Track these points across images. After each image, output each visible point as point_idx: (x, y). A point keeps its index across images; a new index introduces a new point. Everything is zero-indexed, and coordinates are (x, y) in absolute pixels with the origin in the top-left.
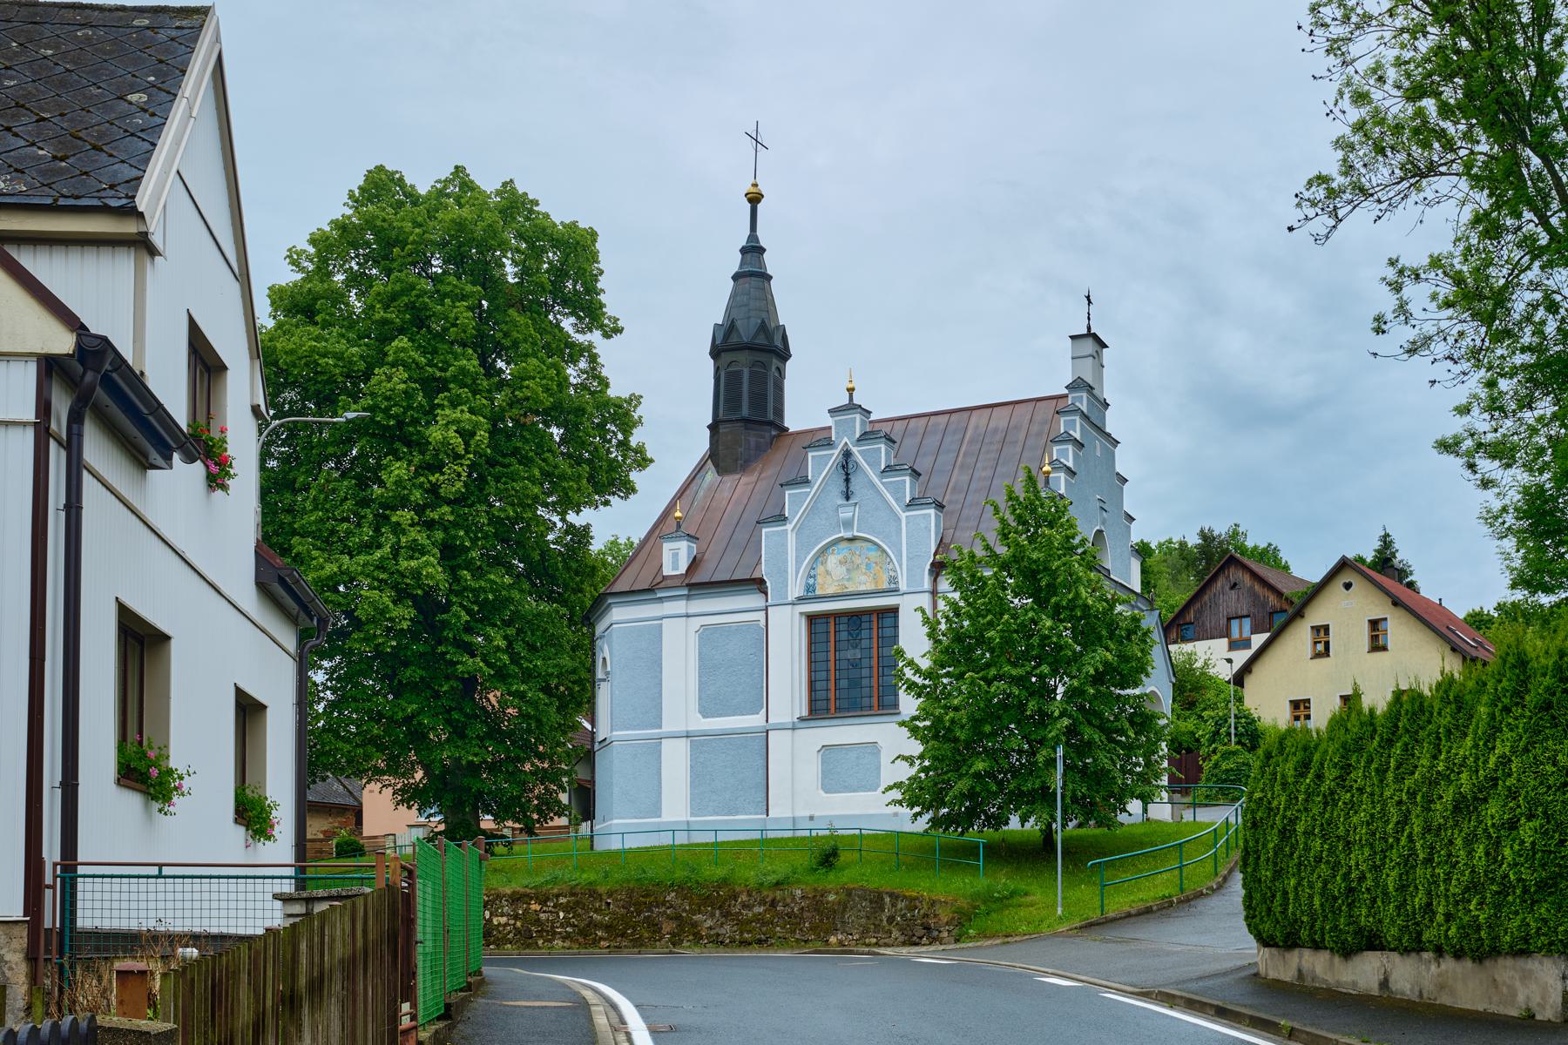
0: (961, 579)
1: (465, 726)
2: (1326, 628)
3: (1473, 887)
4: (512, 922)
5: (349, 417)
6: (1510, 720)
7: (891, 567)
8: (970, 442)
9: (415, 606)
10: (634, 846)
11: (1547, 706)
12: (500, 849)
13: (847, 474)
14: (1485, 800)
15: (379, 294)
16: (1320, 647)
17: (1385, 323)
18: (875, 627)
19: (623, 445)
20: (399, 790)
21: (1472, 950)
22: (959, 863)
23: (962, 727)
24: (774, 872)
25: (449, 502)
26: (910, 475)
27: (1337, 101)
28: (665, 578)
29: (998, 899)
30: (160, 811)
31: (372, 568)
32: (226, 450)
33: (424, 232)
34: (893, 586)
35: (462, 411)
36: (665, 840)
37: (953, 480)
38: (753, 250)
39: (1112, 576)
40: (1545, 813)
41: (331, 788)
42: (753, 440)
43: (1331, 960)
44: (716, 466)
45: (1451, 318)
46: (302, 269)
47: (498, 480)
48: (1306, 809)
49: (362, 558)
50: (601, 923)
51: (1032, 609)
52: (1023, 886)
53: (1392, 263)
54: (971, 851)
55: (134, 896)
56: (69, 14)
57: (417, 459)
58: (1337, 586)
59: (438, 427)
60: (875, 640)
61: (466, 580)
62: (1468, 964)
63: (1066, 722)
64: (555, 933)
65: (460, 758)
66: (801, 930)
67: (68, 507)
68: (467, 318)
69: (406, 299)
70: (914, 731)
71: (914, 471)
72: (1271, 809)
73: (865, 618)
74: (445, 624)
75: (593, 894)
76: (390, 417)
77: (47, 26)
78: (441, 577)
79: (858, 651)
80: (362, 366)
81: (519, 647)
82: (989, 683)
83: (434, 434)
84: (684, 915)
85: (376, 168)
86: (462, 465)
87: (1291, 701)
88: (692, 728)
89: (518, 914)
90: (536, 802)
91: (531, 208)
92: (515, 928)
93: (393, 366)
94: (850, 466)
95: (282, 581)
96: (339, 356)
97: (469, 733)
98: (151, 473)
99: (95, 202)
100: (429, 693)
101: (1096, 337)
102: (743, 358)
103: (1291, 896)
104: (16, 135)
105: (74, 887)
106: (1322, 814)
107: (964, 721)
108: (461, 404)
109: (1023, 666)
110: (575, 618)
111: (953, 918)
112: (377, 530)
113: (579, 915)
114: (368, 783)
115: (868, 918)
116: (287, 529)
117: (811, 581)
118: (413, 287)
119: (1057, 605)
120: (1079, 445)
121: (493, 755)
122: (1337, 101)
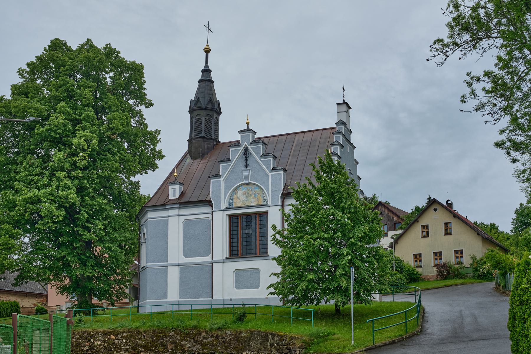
1: (86, 261)
2: (427, 226)
4: (103, 344)
5: (31, 119)
7: (264, 195)
8: (296, 146)
9: (66, 211)
10: (156, 311)
12: (100, 312)
13: (246, 157)
16: (425, 234)
17: (466, 98)
18: (258, 220)
19: (153, 150)
20: (59, 287)
22: (300, 320)
24: (217, 323)
25: (81, 169)
26: (273, 158)
28: (170, 200)
29: (323, 337)
31: (47, 195)
33: (73, 62)
34: (265, 203)
35: (87, 132)
36: (169, 308)
38: (206, 71)
44: (191, 156)
46: (23, 77)
47: (101, 161)
49: (43, 191)
50: (141, 344)
52: (336, 331)
53: (469, 74)
54: (307, 314)
57: (68, 151)
58: (431, 210)
59: (76, 138)
60: (258, 226)
61: (87, 201)
63: (350, 257)
64: (121, 349)
65: (84, 274)
66: (230, 349)
68: (90, 95)
69: (65, 87)
71: (274, 156)
73: (253, 216)
74: (78, 219)
75: (138, 332)
76: (57, 134)
78: (76, 199)
79: (250, 230)
81: (109, 229)
83: (75, 141)
84: (177, 341)
86: (86, 154)
87: (414, 254)
88: (181, 262)
89: (105, 340)
91: (118, 55)
92: (104, 346)
93: (58, 114)
94: (248, 154)
101: (347, 104)
102: (203, 113)
110: (133, 219)
111: (302, 345)
112: (51, 180)
113: (132, 341)
115: (261, 344)
116: (13, 179)
117: (231, 201)
118: (68, 83)
120: (342, 146)
121: (98, 273)
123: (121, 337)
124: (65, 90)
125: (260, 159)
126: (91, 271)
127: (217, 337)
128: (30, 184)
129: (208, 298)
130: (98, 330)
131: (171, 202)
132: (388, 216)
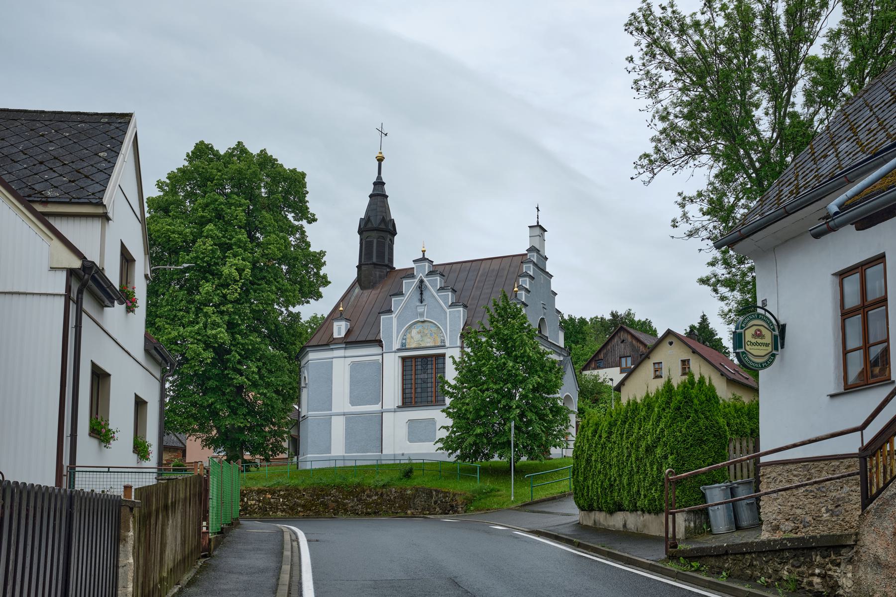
0: (471, 342)
1: (237, 409)
3: (653, 483)
4: (257, 503)
6: (665, 414)
7: (442, 335)
10: (317, 467)
11: (678, 408)
13: (421, 291)
14: (656, 447)
15: (200, 204)
19: (317, 274)
21: (653, 510)
22: (469, 476)
23: (471, 412)
25: (231, 302)
26: (451, 292)
27: (652, 120)
28: (334, 339)
29: (486, 493)
30: (105, 447)
32: (134, 296)
34: (443, 344)
36: (332, 464)
37: (472, 294)
38: (379, 184)
39: (549, 340)
40: (677, 452)
41: (171, 439)
42: (378, 273)
43: (606, 515)
44: (360, 285)
45: (709, 220)
46: (163, 190)
47: (255, 292)
48: (596, 451)
49: (189, 329)
51: (504, 358)
53: (680, 194)
54: (474, 470)
55: (98, 480)
56: (74, 117)
57: (216, 282)
61: (239, 339)
62: (653, 516)
64: (278, 509)
65: (234, 424)
66: (395, 507)
67: (76, 326)
70: (449, 414)
71: (453, 290)
72: (583, 451)
74: (228, 360)
75: (297, 490)
76: (204, 262)
77: (66, 122)
80: (191, 237)
81: (264, 371)
82: (483, 392)
85: (200, 142)
88: (346, 411)
90: (271, 446)
94: (423, 287)
95: (156, 349)
96: (180, 233)
97: (239, 412)
98: (106, 309)
99: (86, 201)
100: (220, 393)
102: (374, 234)
103: (590, 488)
104: (54, 171)
105: (74, 475)
106: (601, 452)
107: (471, 410)
108: (238, 256)
109: (499, 384)
112: (197, 315)
113: (290, 500)
114: (189, 436)
115: (425, 502)
117: (404, 341)
118: (216, 200)
119: (516, 355)
120: (532, 278)
122: (652, 120)
123: (278, 496)
124: (213, 209)
125: (437, 293)
126: (242, 420)
127: (382, 495)
128: (173, 320)
129: (377, 452)
130: (252, 488)
131: (336, 341)
132: (632, 345)
